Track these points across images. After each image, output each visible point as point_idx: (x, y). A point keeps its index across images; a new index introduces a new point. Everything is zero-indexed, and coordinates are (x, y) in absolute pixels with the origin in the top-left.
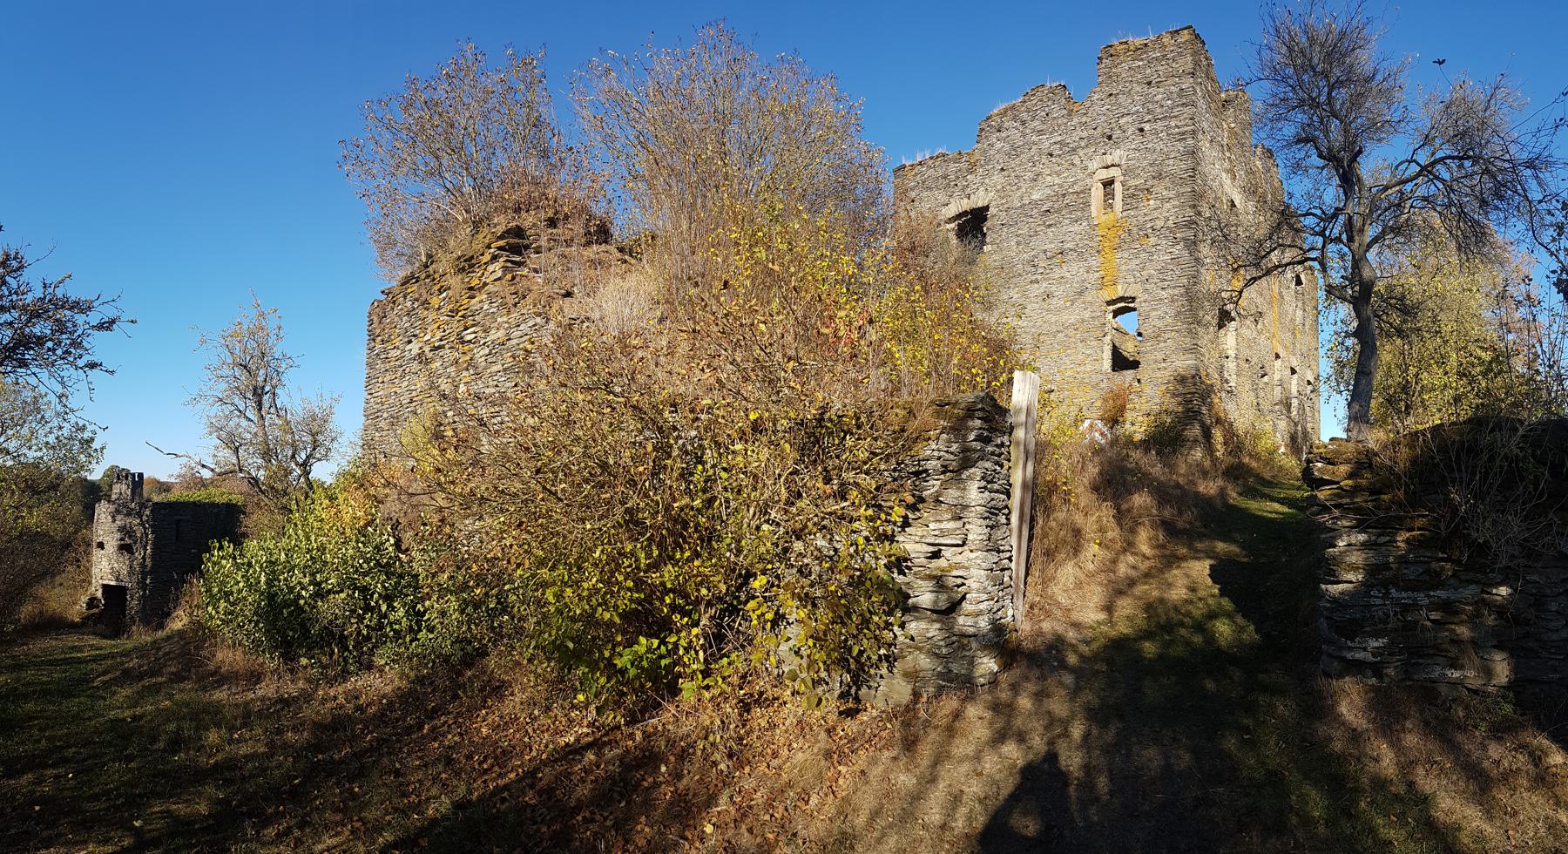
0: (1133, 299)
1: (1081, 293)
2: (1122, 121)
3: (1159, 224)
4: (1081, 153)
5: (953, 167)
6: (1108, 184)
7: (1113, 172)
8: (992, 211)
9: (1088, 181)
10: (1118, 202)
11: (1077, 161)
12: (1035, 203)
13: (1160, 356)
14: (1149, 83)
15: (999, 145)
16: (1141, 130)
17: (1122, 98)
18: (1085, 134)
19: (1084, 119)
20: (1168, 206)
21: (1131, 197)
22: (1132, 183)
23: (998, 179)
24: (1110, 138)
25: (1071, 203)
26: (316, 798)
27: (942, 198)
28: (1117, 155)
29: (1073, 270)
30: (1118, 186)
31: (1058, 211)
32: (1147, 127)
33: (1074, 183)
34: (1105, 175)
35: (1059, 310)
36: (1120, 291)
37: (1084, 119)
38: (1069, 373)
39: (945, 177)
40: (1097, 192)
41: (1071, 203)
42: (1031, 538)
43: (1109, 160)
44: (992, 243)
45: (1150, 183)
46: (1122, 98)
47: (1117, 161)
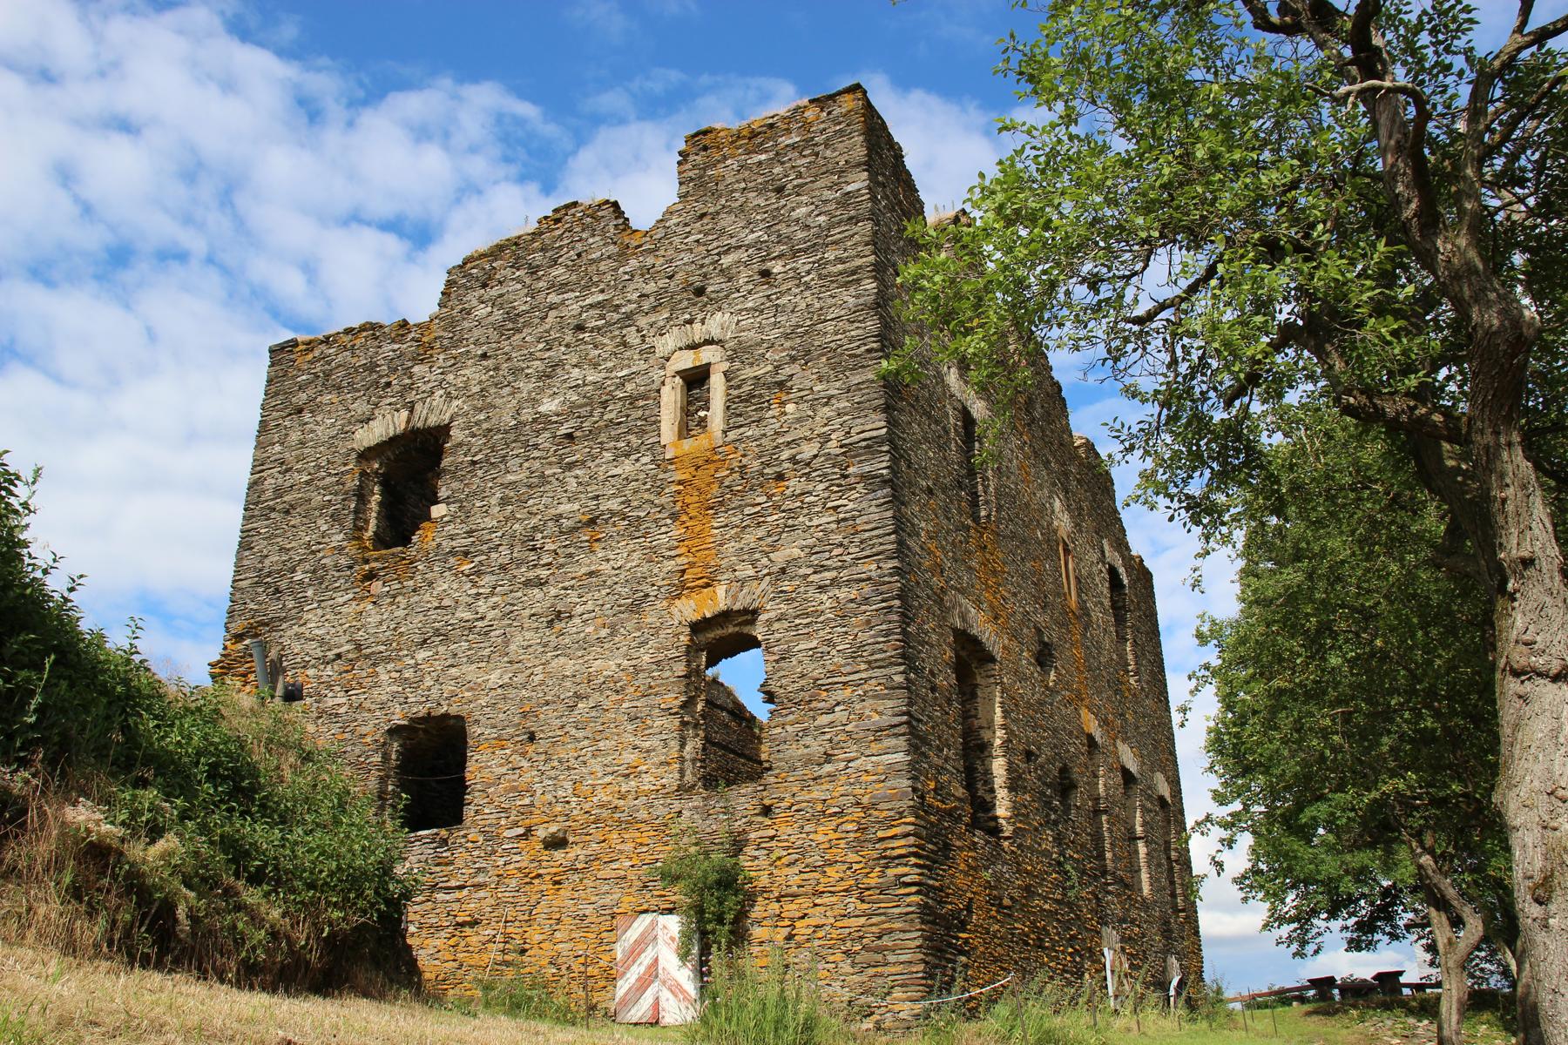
0: (751, 614)
1: (635, 608)
2: (726, 261)
3: (808, 450)
4: (643, 322)
5: (388, 349)
6: (696, 379)
7: (708, 355)
8: (457, 434)
9: (657, 374)
10: (716, 415)
11: (633, 338)
12: (543, 421)
13: (816, 747)
14: (780, 190)
15: (482, 311)
16: (766, 274)
17: (726, 221)
18: (651, 287)
19: (650, 260)
20: (826, 411)
21: (744, 403)
22: (749, 372)
23: (473, 373)
24: (700, 292)
25: (617, 418)
26: (883, 175)
27: (361, 407)
28: (717, 323)
29: (618, 558)
30: (717, 382)
31: (593, 433)
32: (777, 268)
33: (624, 381)
34: (687, 360)
35: (585, 644)
36: (721, 598)
37: (650, 260)
38: (602, 796)
39: (372, 367)
40: (671, 397)
41: (617, 418)
42: (878, 537)
43: (698, 332)
44: (447, 501)
45: (787, 370)
46: (726, 221)
47: (716, 333)
